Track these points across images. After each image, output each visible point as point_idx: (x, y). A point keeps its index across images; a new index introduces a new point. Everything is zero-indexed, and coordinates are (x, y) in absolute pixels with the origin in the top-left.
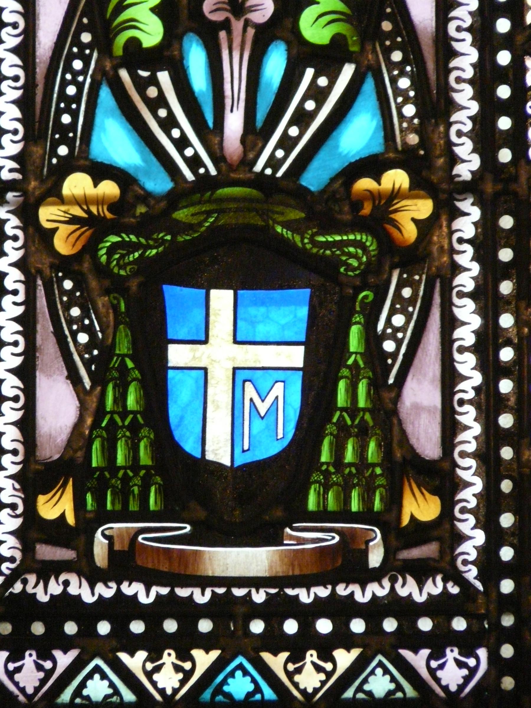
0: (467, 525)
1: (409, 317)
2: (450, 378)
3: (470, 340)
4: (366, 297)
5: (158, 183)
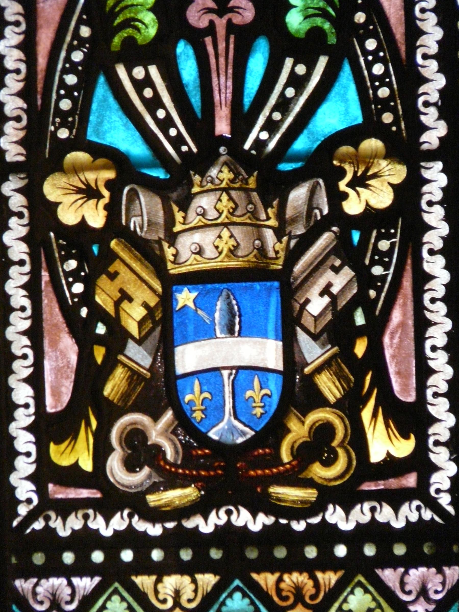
2: (422, 324)
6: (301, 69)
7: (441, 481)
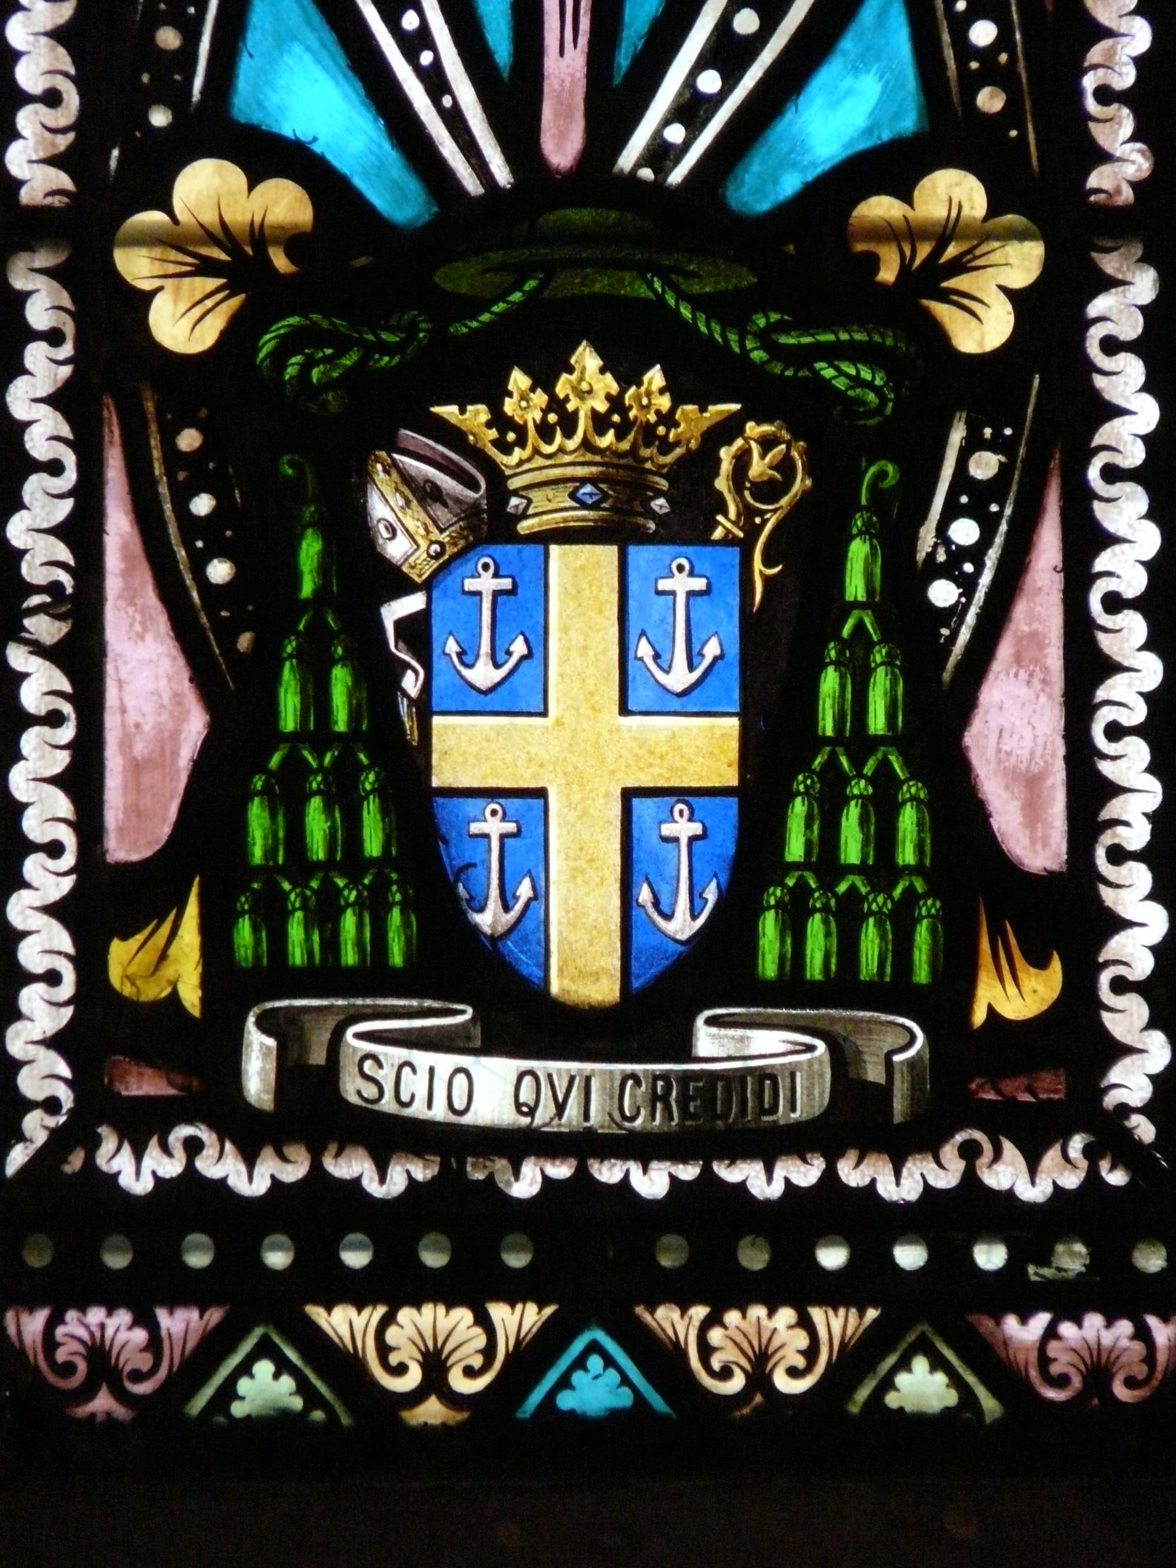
1: (988, 527)
2: (1087, 666)
3: (1134, 583)
4: (882, 475)
5: (393, 194)
7: (1131, 1083)
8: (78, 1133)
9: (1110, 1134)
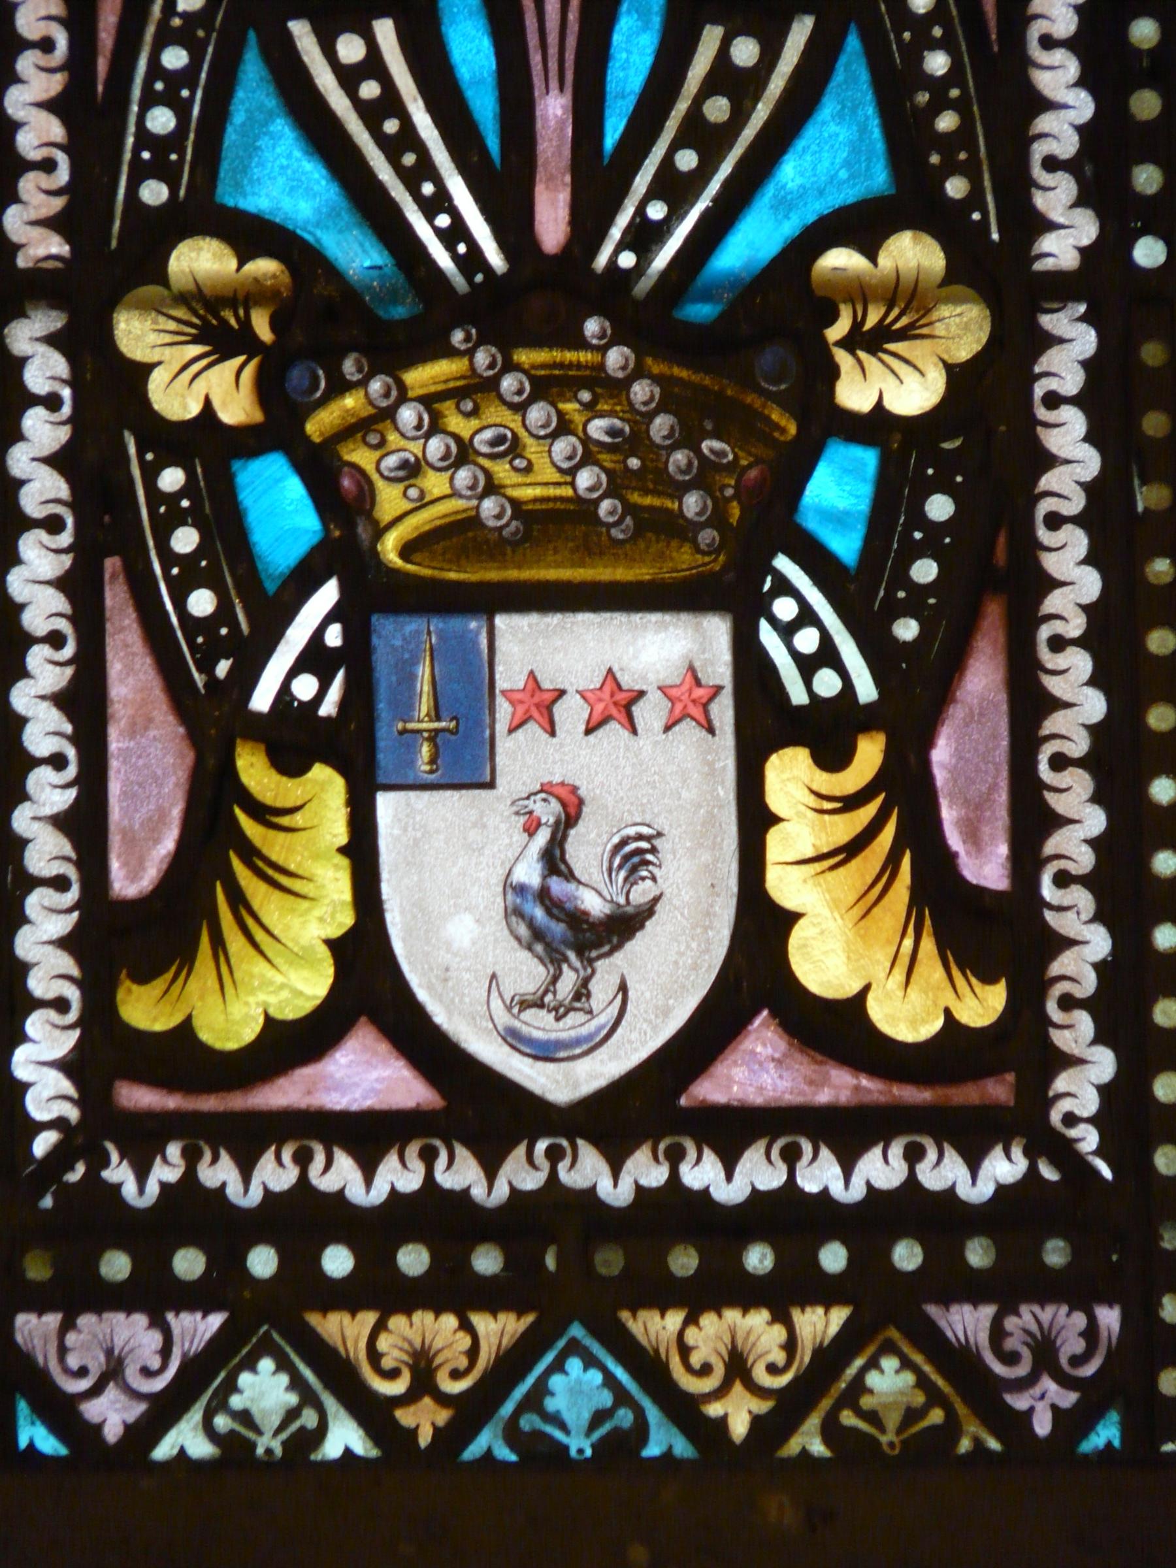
0: (1076, 1032)
6: (745, 52)
8: (81, 1141)
9: (1048, 1143)
